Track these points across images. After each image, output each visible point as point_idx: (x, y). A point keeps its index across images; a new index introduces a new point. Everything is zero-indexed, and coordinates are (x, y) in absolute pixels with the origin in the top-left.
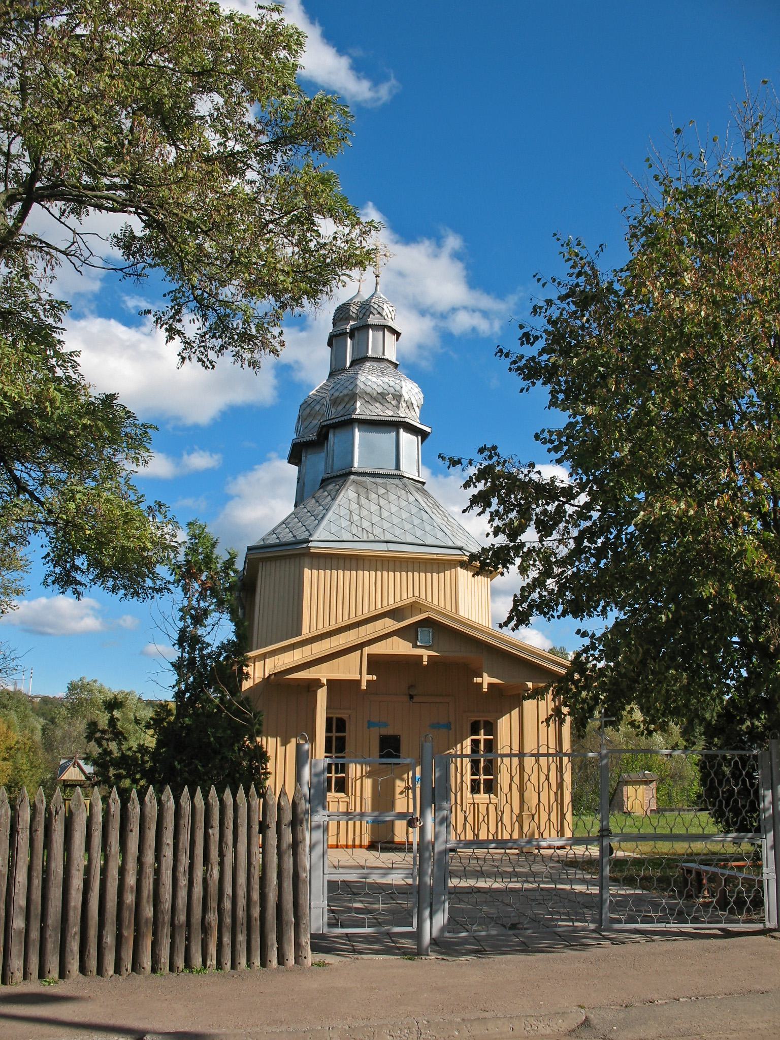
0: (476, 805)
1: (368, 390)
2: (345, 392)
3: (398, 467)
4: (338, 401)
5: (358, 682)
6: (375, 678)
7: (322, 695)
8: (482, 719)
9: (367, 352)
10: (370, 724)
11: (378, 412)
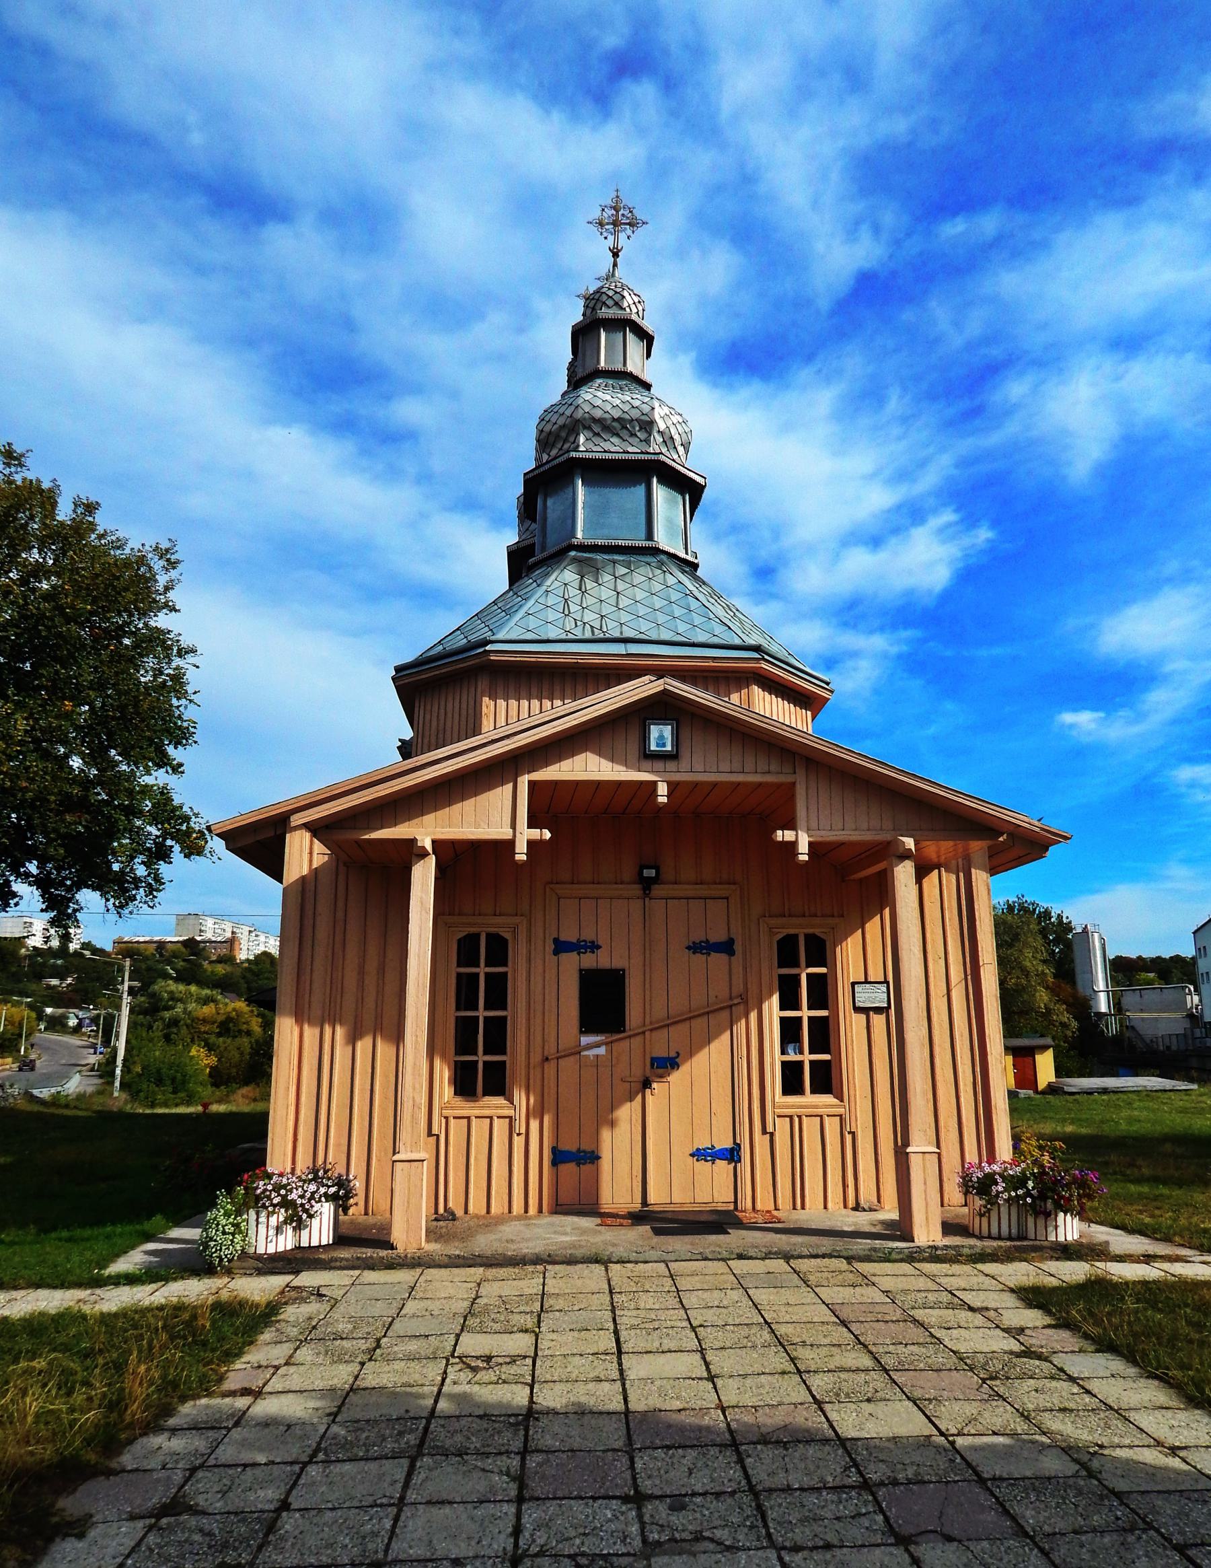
0: (796, 1120)
1: (598, 414)
2: (561, 421)
3: (650, 536)
4: (552, 439)
5: (510, 844)
6: (547, 835)
7: (424, 877)
8: (801, 933)
9: (598, 362)
10: (561, 947)
11: (613, 448)
